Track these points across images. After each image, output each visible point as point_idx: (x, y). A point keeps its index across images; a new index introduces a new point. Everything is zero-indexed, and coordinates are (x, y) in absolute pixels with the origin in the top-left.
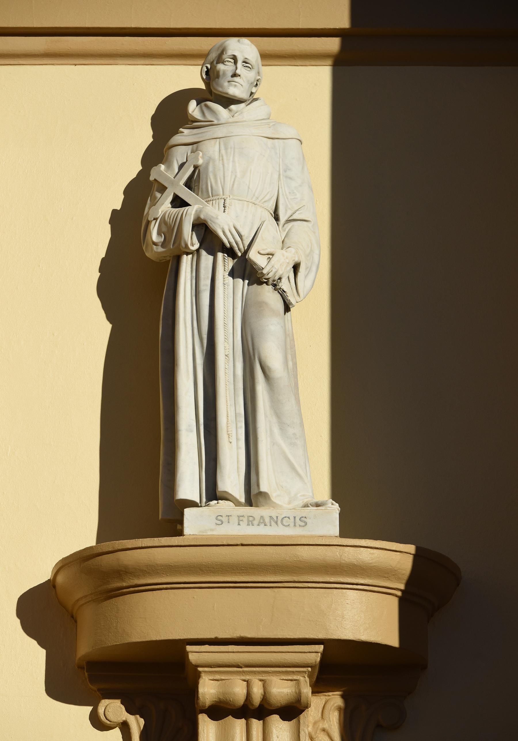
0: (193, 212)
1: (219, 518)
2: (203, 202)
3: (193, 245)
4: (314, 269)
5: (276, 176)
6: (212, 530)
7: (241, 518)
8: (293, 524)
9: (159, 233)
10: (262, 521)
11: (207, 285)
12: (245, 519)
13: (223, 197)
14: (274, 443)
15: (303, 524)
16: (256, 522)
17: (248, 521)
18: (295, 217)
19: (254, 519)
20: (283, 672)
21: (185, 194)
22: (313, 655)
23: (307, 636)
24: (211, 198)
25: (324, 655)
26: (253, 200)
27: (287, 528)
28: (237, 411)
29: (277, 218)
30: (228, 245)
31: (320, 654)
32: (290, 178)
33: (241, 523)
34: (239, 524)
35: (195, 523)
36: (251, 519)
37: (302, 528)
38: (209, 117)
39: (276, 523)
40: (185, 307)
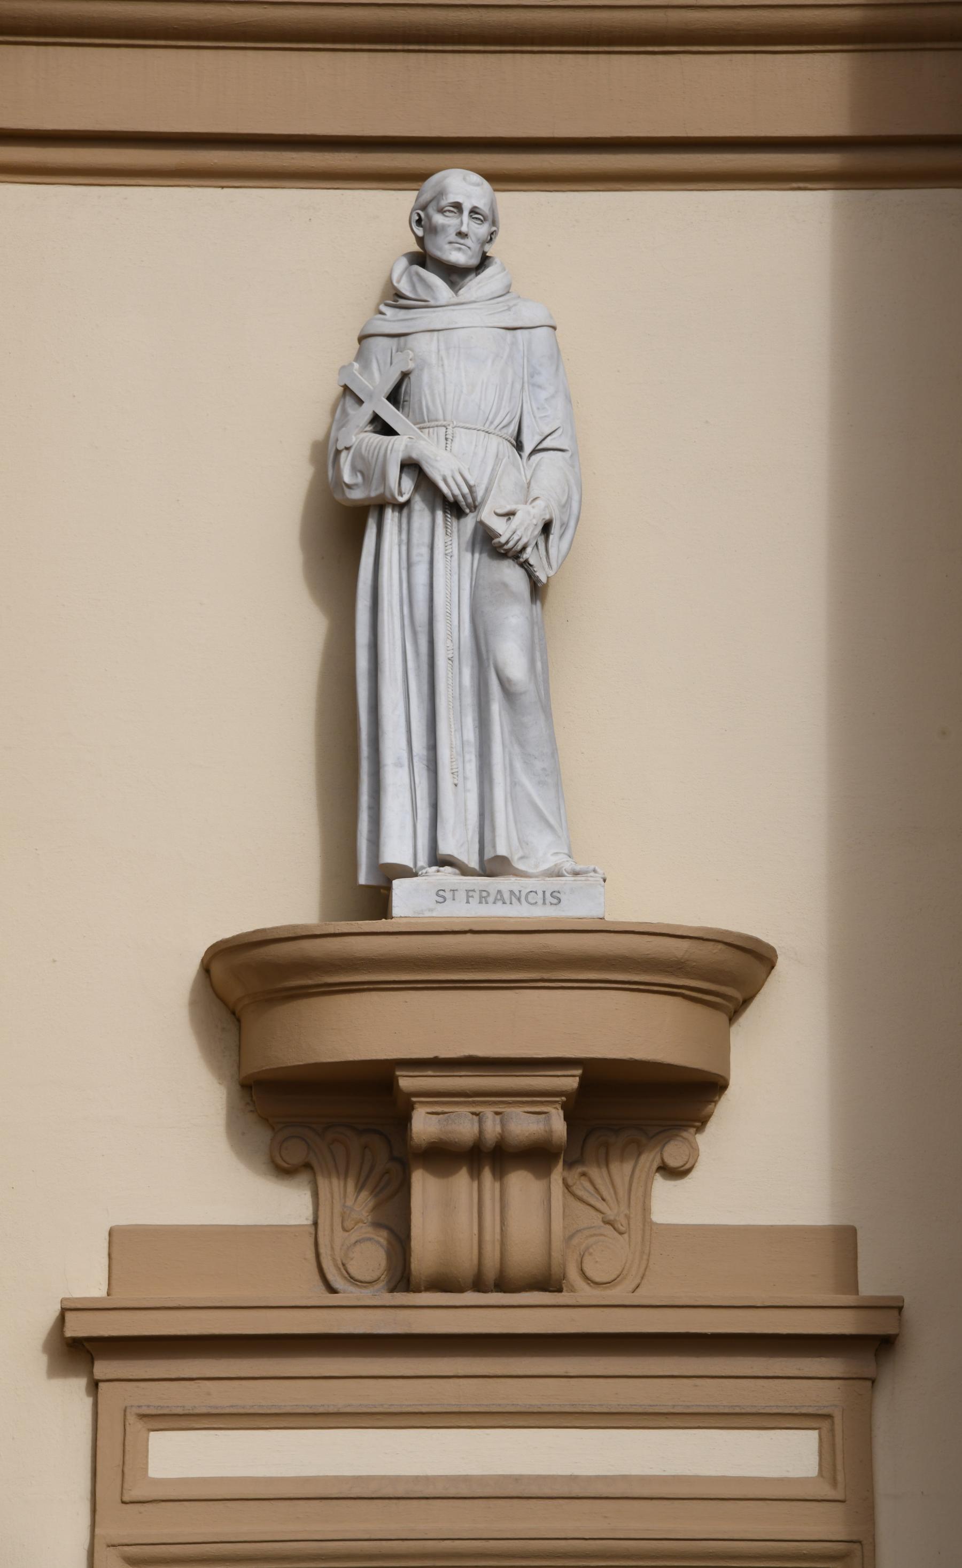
0: (402, 448)
1: (441, 893)
2: (414, 430)
3: (401, 494)
4: (572, 523)
5: (518, 386)
6: (431, 910)
7: (471, 894)
8: (542, 901)
9: (354, 469)
10: (499, 897)
11: (422, 555)
12: (476, 895)
13: (444, 423)
14: (514, 783)
15: (555, 901)
16: (491, 899)
17: (481, 897)
18: (545, 445)
19: (489, 894)
20: (523, 1103)
21: (390, 414)
22: (570, 1081)
23: (324, 59)
24: (427, 424)
25: (582, 1078)
26: (486, 428)
27: (533, 907)
28: (465, 738)
29: (519, 446)
30: (451, 499)
31: (577, 1079)
32: (540, 387)
33: (471, 899)
34: (468, 902)
35: (408, 901)
36: (484, 894)
37: (554, 907)
38: (423, 294)
39: (519, 900)
40: (391, 585)
